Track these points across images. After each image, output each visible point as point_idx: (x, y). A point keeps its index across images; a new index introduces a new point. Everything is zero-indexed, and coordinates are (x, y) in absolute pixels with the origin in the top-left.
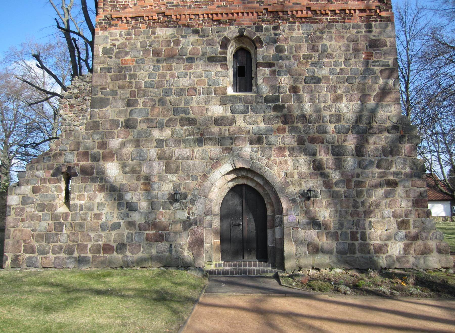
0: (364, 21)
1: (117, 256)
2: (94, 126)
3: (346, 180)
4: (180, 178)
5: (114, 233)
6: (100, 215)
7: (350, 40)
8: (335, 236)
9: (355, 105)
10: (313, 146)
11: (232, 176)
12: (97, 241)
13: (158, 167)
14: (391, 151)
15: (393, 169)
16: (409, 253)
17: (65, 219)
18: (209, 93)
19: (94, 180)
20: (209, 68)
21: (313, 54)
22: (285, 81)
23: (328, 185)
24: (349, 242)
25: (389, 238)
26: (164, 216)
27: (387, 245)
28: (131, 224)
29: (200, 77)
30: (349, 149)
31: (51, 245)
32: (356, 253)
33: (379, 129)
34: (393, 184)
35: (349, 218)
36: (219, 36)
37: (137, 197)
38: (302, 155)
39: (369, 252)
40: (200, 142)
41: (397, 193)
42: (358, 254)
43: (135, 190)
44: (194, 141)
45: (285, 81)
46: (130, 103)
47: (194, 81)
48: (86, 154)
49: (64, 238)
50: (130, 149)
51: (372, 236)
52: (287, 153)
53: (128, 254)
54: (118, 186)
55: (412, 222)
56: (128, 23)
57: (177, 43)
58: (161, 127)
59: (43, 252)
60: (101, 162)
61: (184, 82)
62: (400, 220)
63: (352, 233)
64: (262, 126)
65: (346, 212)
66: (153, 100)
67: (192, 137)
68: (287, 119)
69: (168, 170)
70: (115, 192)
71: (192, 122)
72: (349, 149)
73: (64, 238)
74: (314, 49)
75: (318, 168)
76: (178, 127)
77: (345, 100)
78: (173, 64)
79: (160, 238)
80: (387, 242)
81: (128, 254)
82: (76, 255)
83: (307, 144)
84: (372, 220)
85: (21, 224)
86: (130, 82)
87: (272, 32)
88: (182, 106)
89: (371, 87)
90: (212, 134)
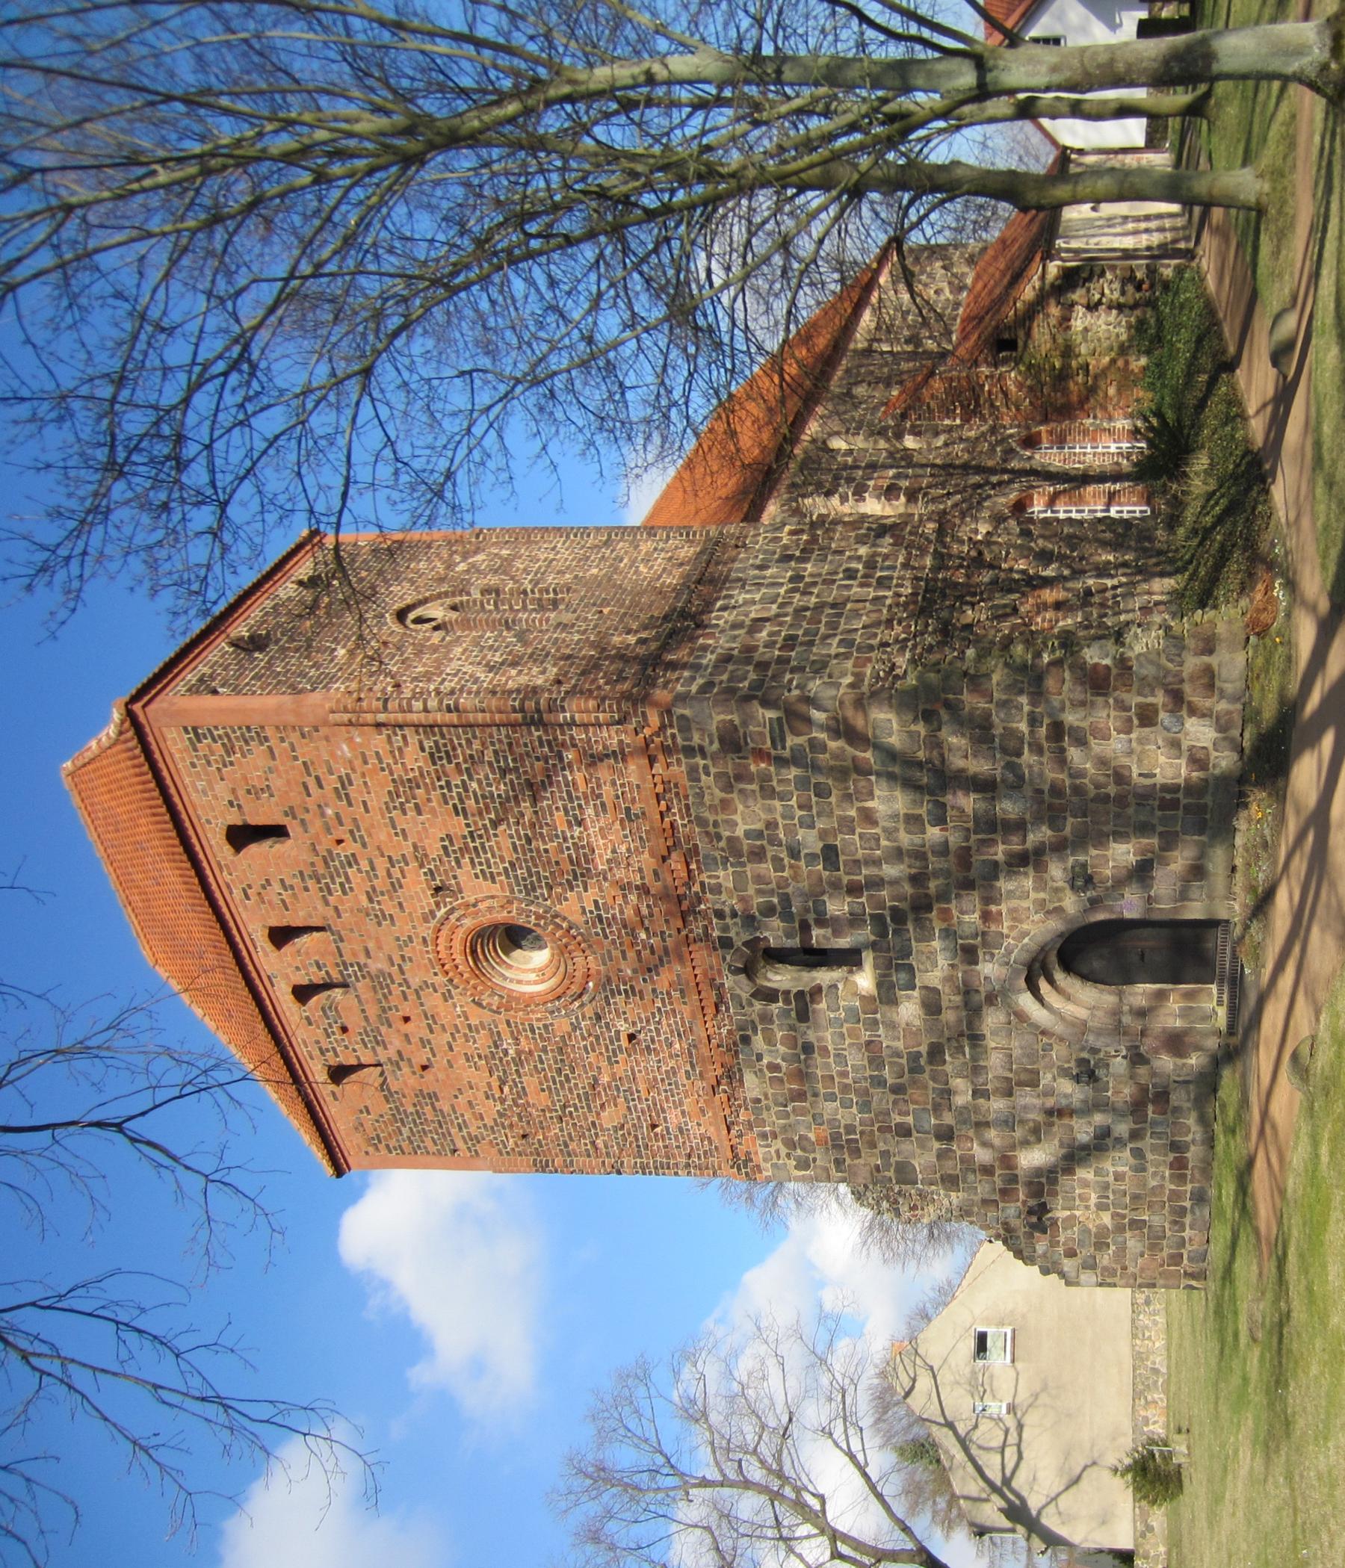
0: (679, 761)
1: (1194, 1154)
2: (951, 1182)
3: (1052, 815)
4: (1049, 1067)
5: (1150, 1156)
6: (1116, 1173)
7: (728, 788)
8: (1169, 842)
9: (881, 790)
10: (975, 865)
11: (1044, 986)
12: (1163, 1177)
13: (1026, 1098)
14: (981, 731)
15: (1023, 727)
16: (1211, 710)
17: (1124, 1217)
18: (875, 1022)
19: (1053, 1181)
20: (824, 1023)
21: (769, 855)
22: (837, 907)
23: (1059, 847)
24: (1180, 813)
25: (1175, 744)
26: (1121, 1090)
27: (1191, 748)
28: (1135, 1135)
29: (842, 1036)
30: (982, 806)
31: (1168, 1233)
32: (1203, 811)
33: (932, 749)
34: (1058, 730)
35: (1130, 811)
36: (751, 1005)
37: (1083, 1131)
38: (998, 884)
39: (1206, 780)
40: (976, 1039)
41: (1076, 724)
42: (1208, 800)
43: (1072, 1129)
44: (973, 1046)
45: (837, 907)
46: (904, 1132)
47: (851, 1045)
48: (1005, 1193)
49: (1158, 1220)
50: (992, 1134)
51: (1170, 772)
52: (993, 908)
53: (1189, 1138)
54: (1063, 1151)
55: (1140, 699)
56: (740, 1136)
57: (774, 1067)
58: (948, 1093)
59: (1182, 1243)
60: (1018, 1172)
61: (856, 1059)
62: (1136, 722)
63: (1161, 808)
64: (936, 944)
65: (1118, 816)
66: (895, 1102)
67: (967, 1050)
68: (921, 906)
69: (1034, 1083)
70: (1075, 1156)
71: (936, 1053)
72: (982, 806)
73: (1158, 1220)
74: (758, 855)
75: (1021, 861)
76: (948, 1068)
77: (869, 804)
78: (819, 1073)
79: (1162, 1097)
80: (1184, 747)
81: (1189, 1138)
82: (1188, 1204)
83: (973, 874)
84: (1135, 771)
85: (1131, 1270)
86: (862, 1133)
87: (728, 920)
88: (904, 1061)
89: (835, 756)
90: (960, 1021)
